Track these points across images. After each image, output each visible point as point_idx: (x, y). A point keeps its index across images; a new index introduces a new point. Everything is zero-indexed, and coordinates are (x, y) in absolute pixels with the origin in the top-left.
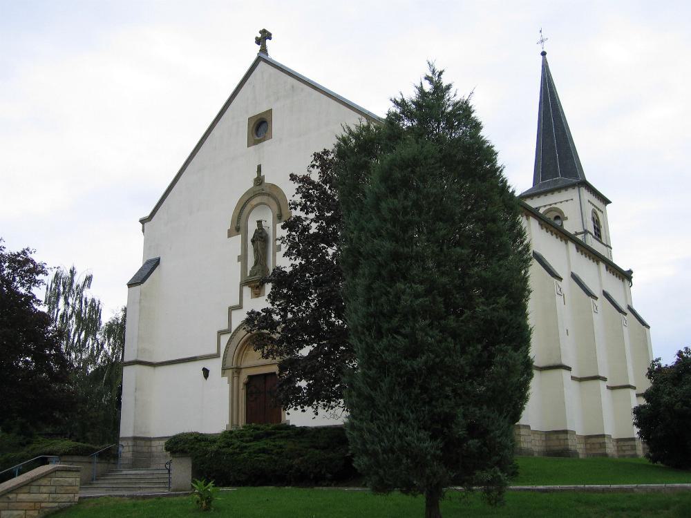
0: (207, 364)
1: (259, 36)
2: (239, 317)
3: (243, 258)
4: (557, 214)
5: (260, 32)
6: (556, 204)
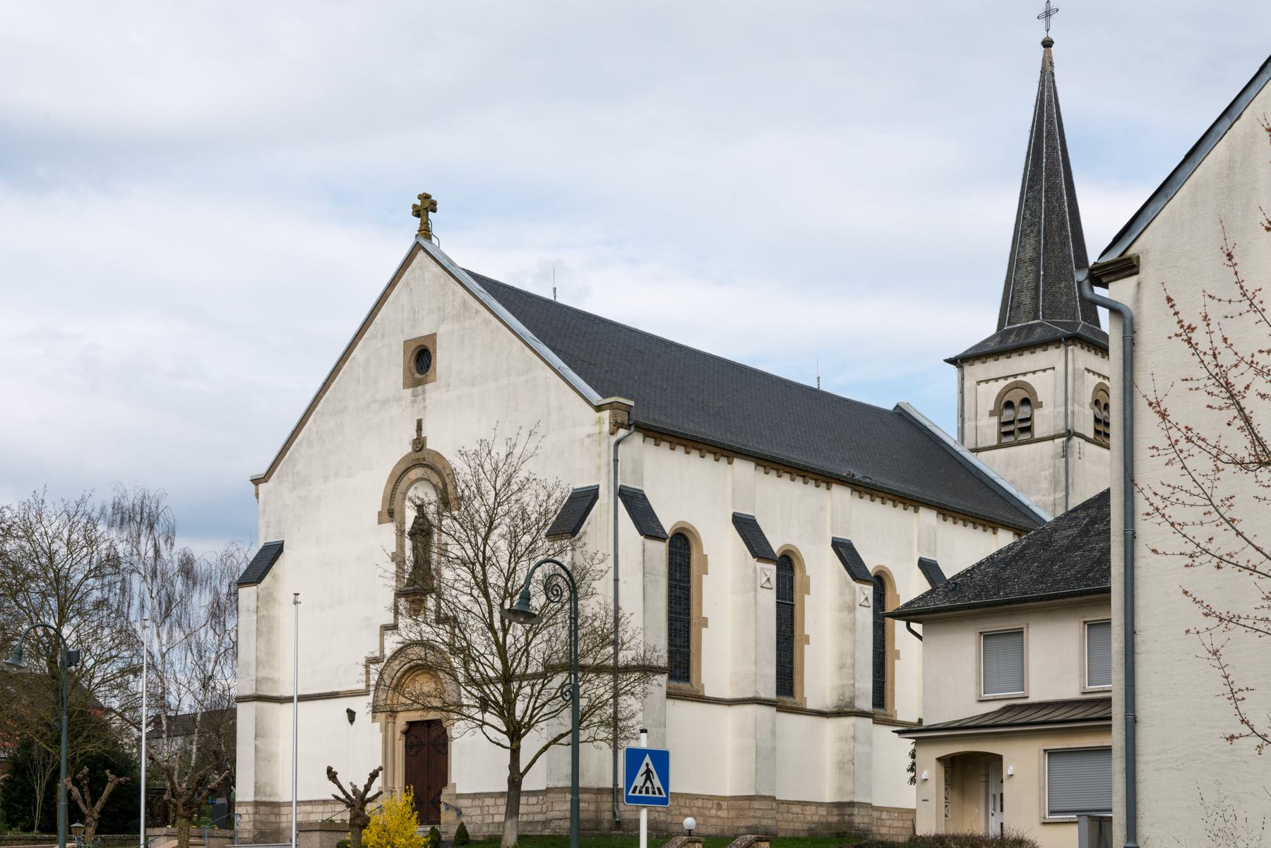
0: (354, 703)
1: (418, 202)
2: (392, 643)
3: (398, 558)
4: (1025, 395)
5: (420, 197)
6: (1025, 374)
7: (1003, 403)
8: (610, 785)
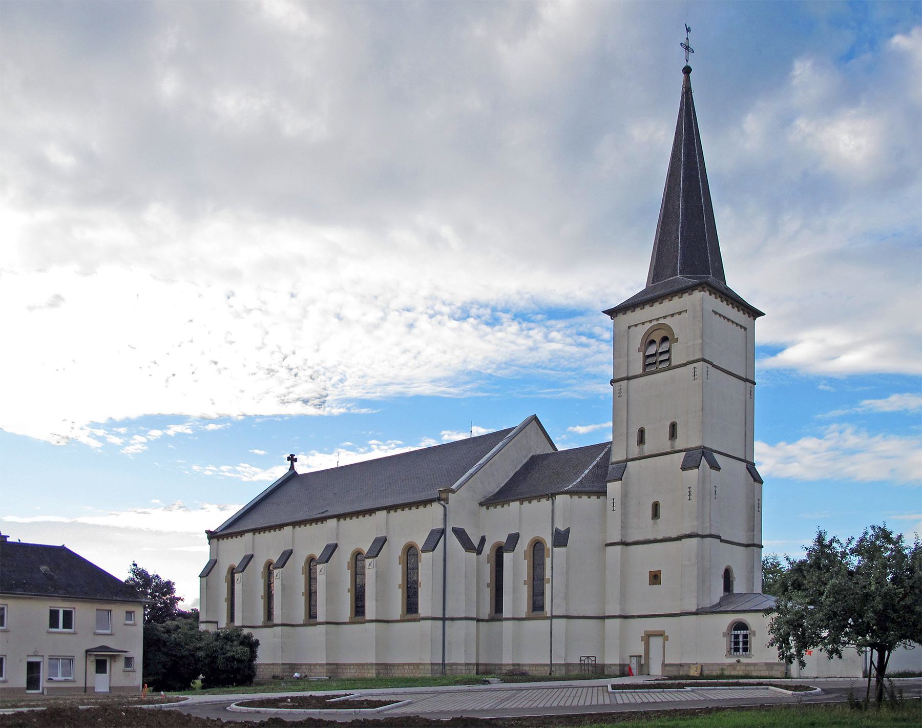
4: (664, 333)
6: (665, 317)
7: (647, 342)
8: (441, 662)
